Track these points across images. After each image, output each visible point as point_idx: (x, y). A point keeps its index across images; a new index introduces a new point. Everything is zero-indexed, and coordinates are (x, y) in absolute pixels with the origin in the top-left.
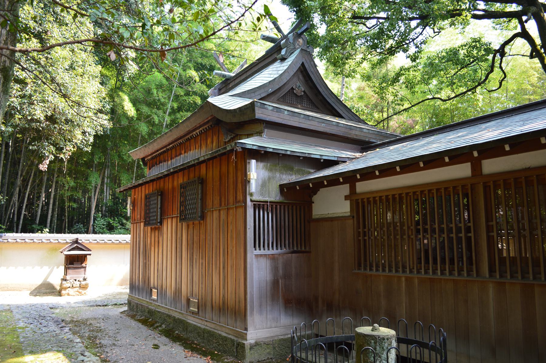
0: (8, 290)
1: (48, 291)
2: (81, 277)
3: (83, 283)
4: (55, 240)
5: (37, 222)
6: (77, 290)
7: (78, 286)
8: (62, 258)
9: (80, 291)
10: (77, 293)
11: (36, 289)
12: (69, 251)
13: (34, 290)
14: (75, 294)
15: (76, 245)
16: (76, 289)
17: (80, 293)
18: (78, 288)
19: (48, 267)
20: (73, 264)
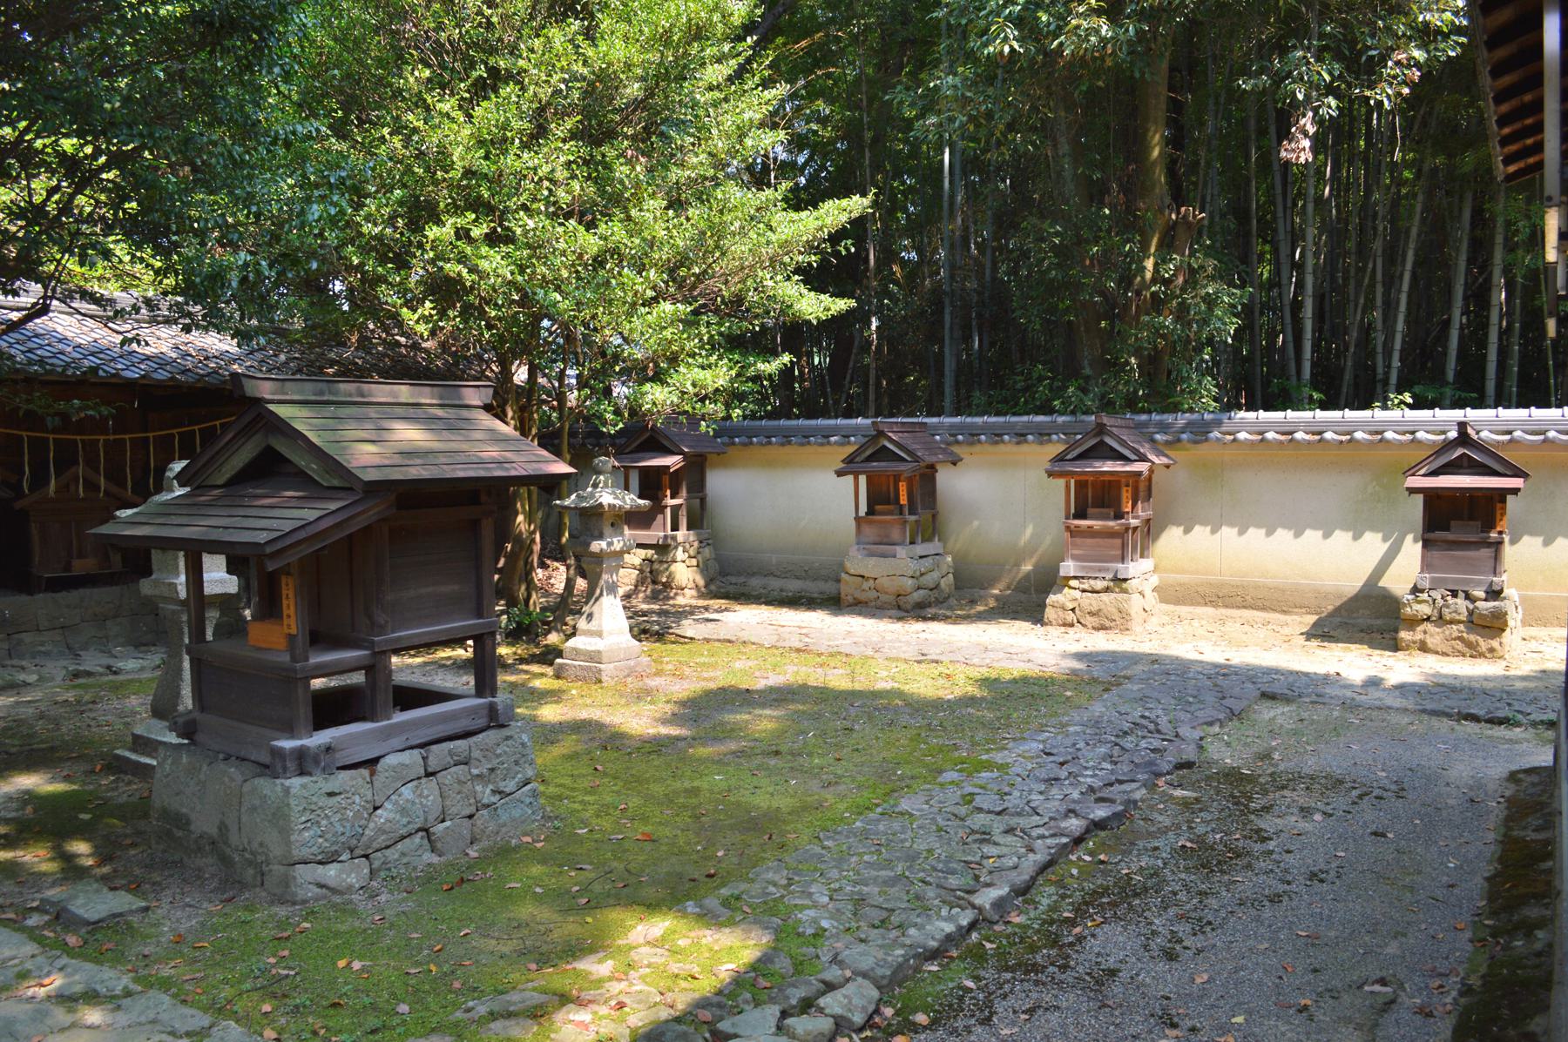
0: (1245, 607)
1: (1379, 622)
2: (1478, 584)
3: (1485, 606)
4: (1404, 433)
5: (1450, 376)
6: (1456, 634)
7: (1464, 617)
8: (1415, 508)
9: (1472, 638)
10: (1459, 645)
11: (1338, 610)
12: (1434, 473)
13: (1331, 615)
14: (1449, 650)
15: (1460, 451)
16: (1454, 629)
17: (1469, 645)
18: (1462, 627)
19: (1380, 535)
20: (1447, 529)
